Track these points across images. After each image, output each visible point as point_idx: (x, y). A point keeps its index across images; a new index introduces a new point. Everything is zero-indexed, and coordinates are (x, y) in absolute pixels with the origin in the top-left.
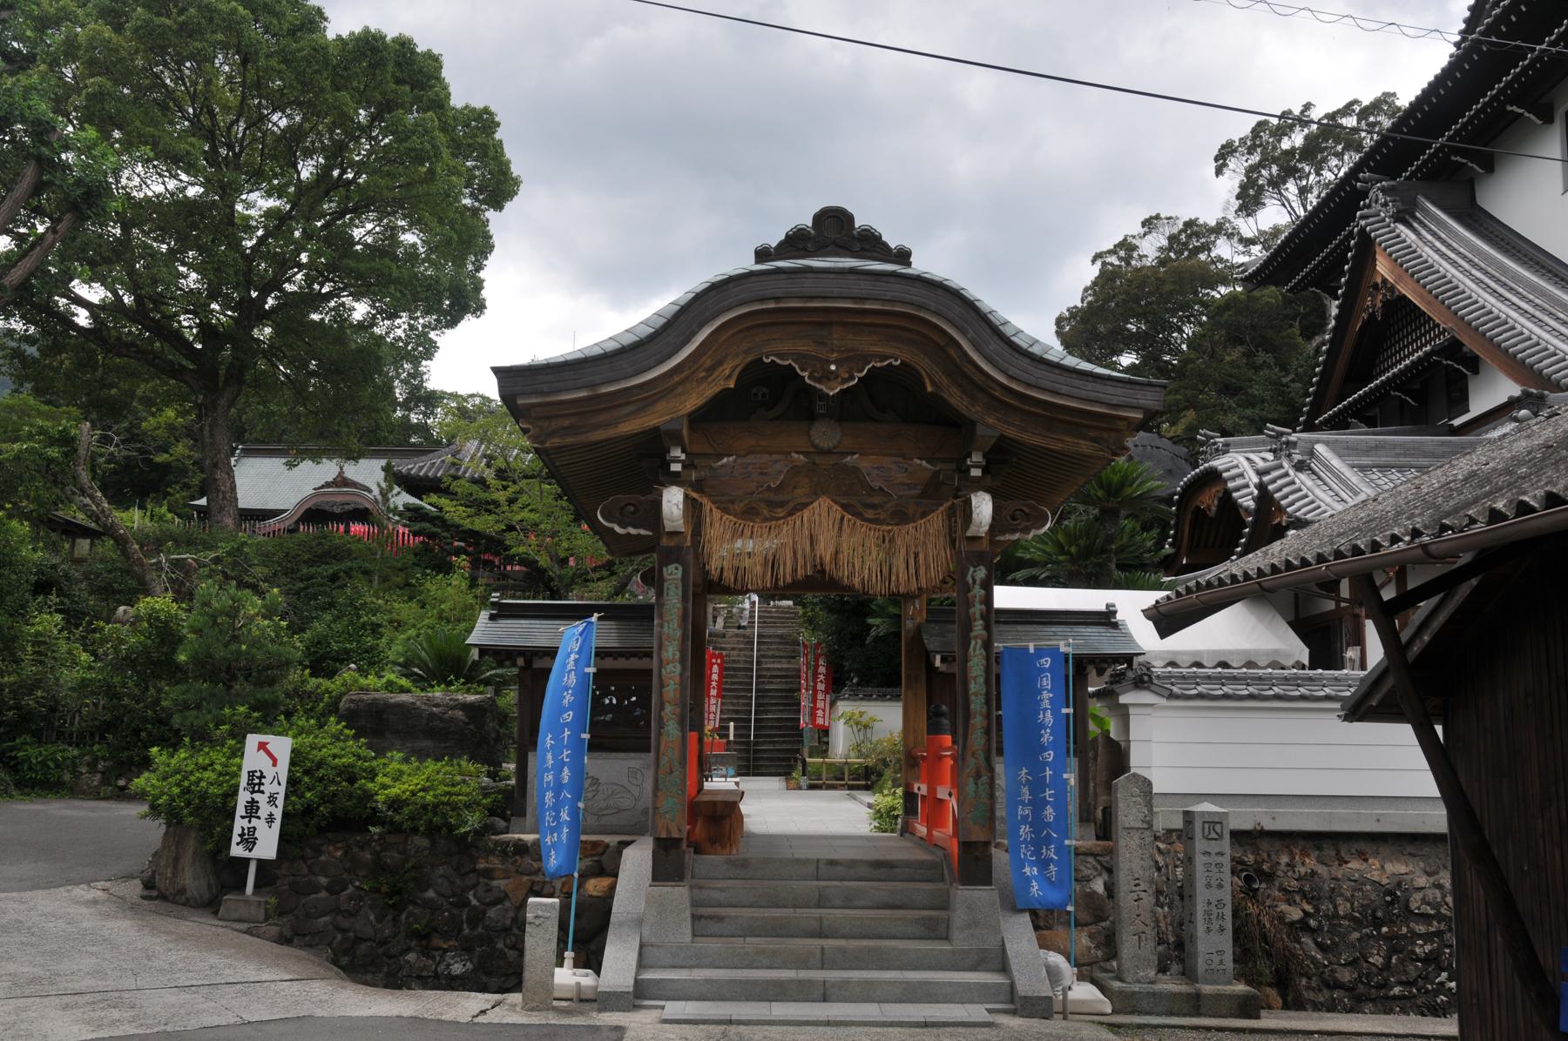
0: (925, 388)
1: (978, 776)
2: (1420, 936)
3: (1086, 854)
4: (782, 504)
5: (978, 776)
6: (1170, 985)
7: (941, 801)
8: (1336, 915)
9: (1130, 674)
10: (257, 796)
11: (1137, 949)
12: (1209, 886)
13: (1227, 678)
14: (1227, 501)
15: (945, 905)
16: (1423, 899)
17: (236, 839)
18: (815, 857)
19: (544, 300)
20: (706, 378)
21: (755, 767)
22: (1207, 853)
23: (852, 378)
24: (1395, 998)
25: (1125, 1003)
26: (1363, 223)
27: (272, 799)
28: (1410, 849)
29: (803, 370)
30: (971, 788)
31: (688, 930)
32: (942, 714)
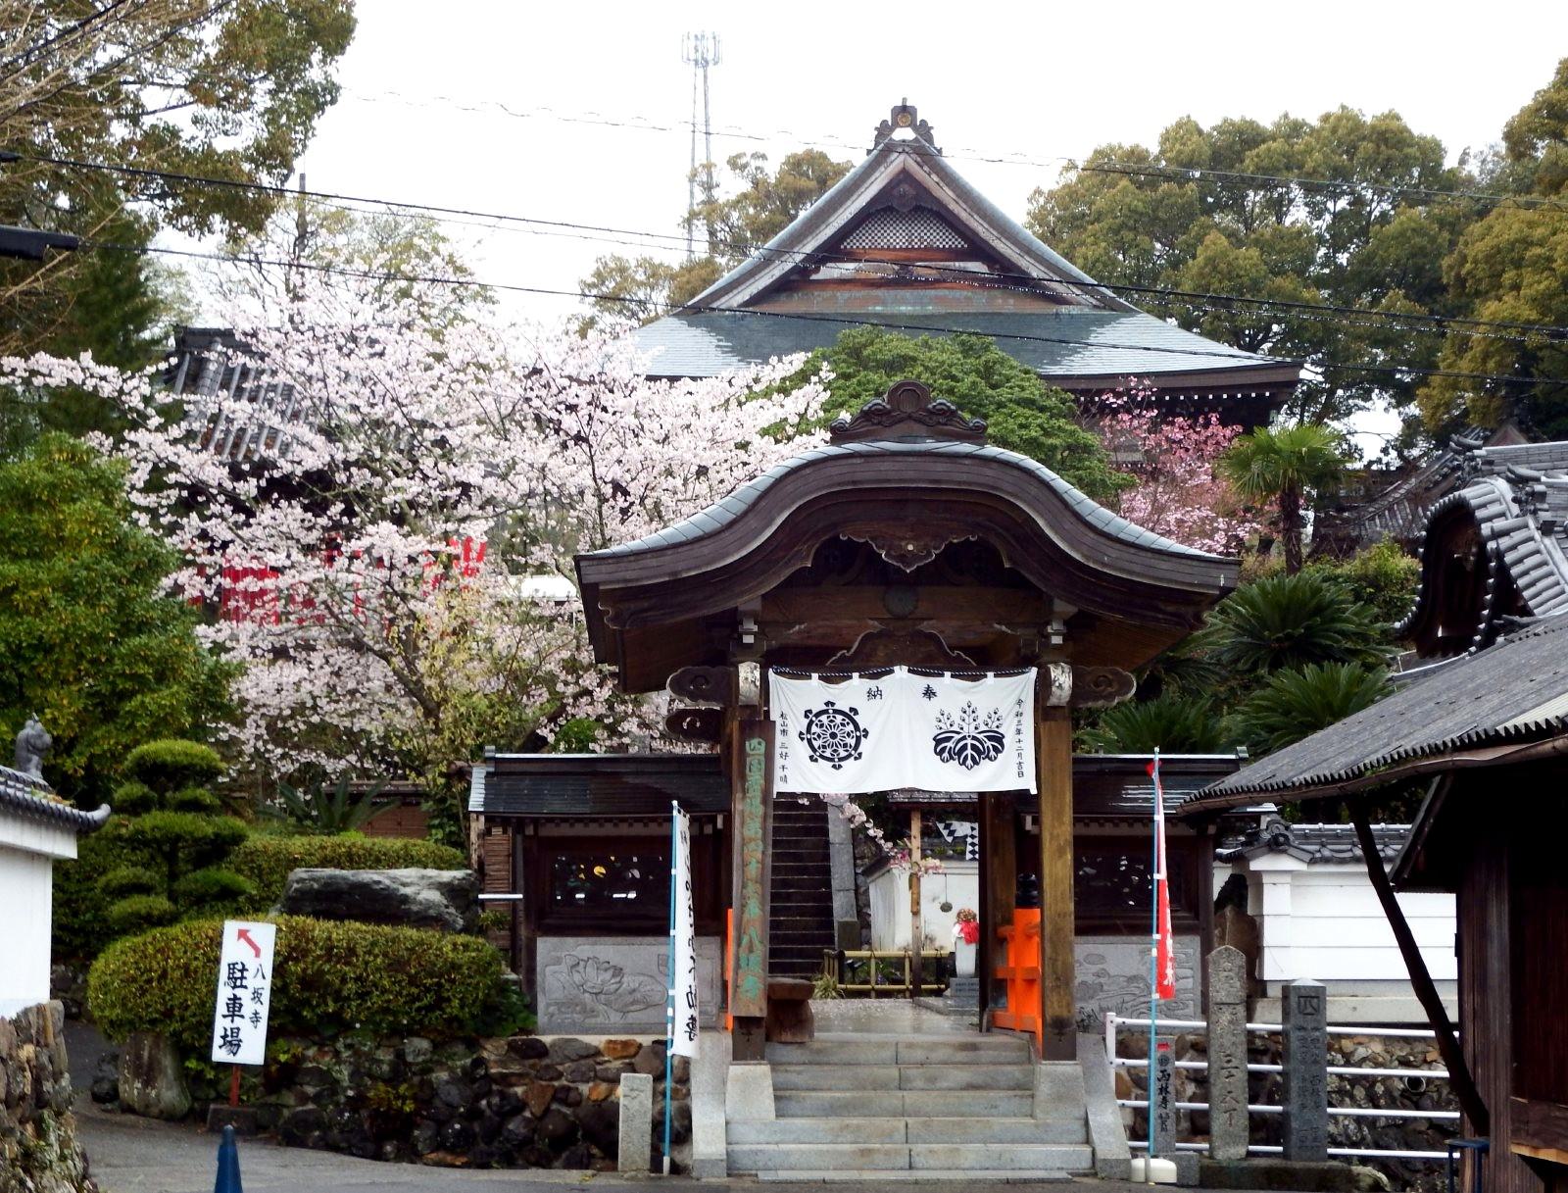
10: (239, 992)
13: (1391, 837)
17: (217, 1041)
27: (256, 996)
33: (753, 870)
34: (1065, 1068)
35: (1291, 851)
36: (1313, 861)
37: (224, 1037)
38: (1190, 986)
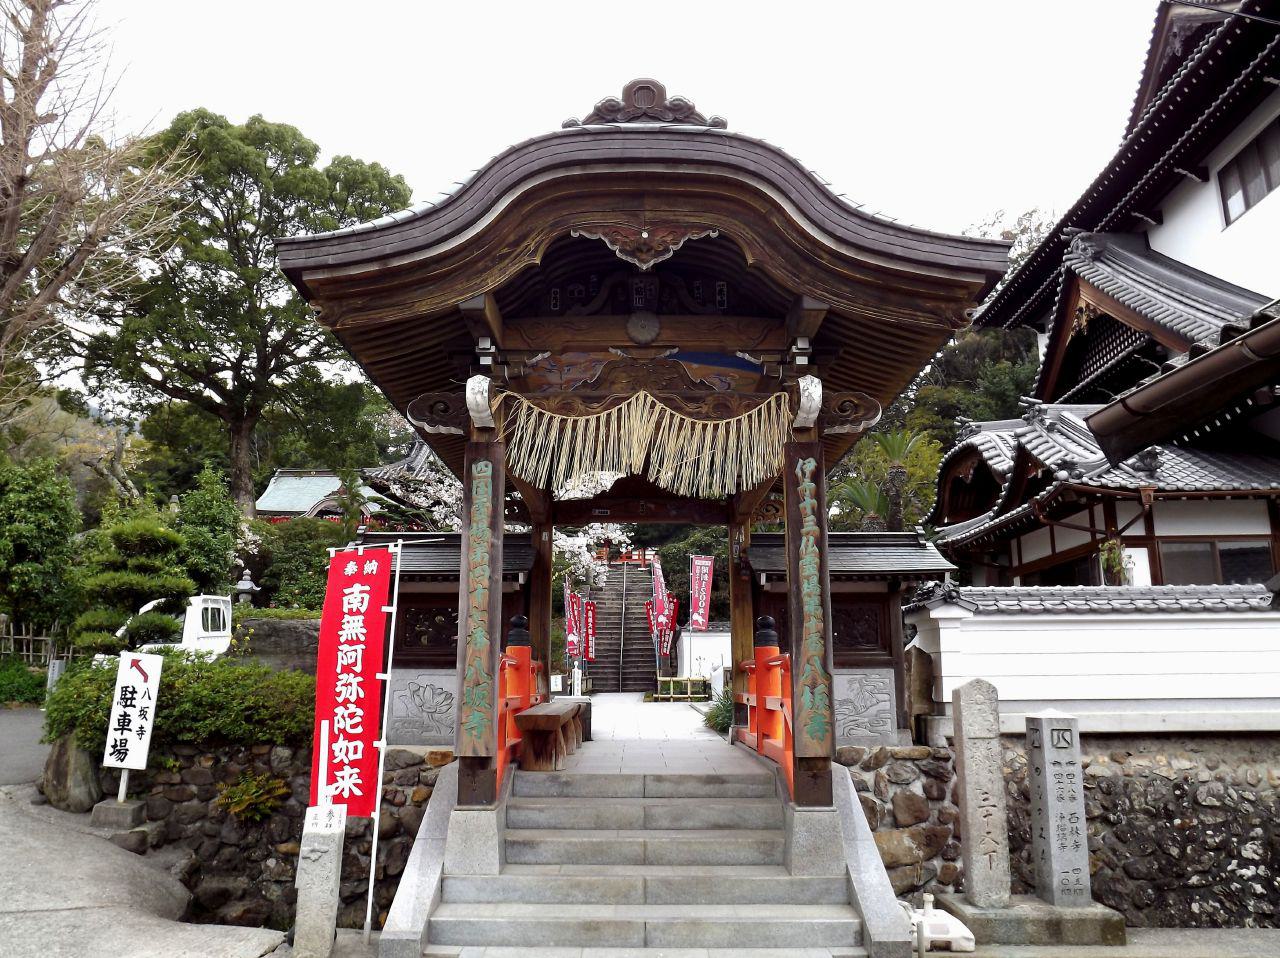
0: (745, 260)
1: (813, 686)
2: (1209, 827)
3: (905, 759)
4: (598, 399)
5: (813, 686)
6: (1028, 909)
7: (771, 712)
8: (1132, 809)
9: (939, 592)
10: (129, 710)
11: (987, 864)
12: (1061, 798)
14: (983, 467)
15: (782, 826)
16: (1209, 792)
17: (109, 749)
18: (642, 773)
19: (321, 164)
20: (509, 254)
21: (624, 685)
22: (1056, 763)
23: (668, 251)
24: (1194, 887)
25: (985, 933)
26: (1068, 263)
27: (143, 713)
28: (1191, 745)
29: (613, 243)
30: (807, 697)
31: (494, 856)
32: (768, 626)
33: (480, 597)
34: (819, 814)
35: (961, 603)
36: (977, 612)
37: (114, 746)
38: (888, 707)
